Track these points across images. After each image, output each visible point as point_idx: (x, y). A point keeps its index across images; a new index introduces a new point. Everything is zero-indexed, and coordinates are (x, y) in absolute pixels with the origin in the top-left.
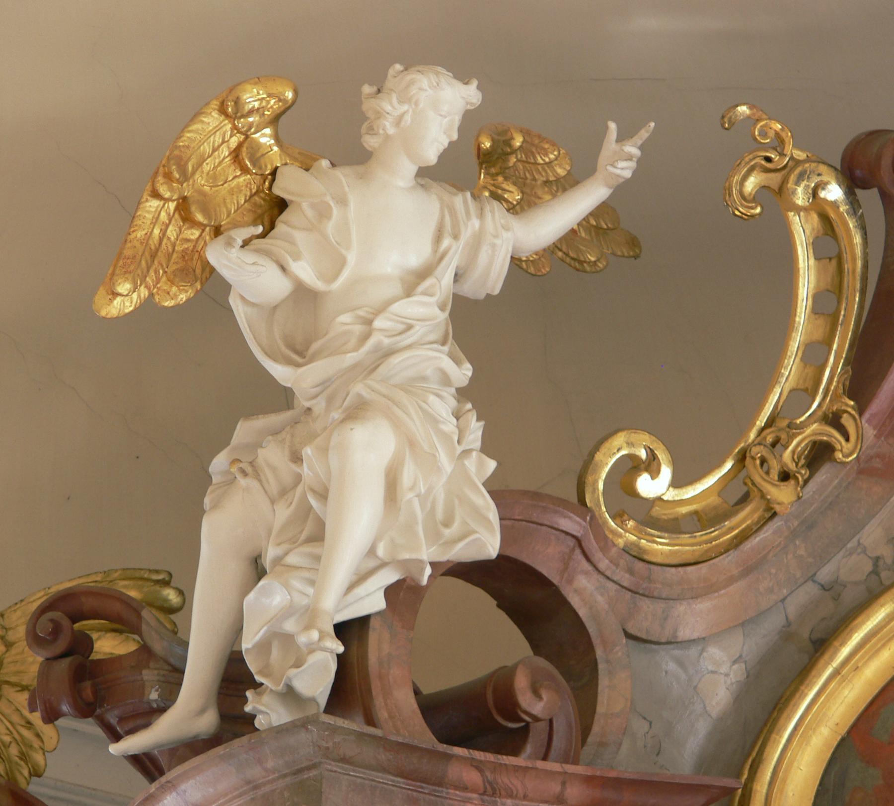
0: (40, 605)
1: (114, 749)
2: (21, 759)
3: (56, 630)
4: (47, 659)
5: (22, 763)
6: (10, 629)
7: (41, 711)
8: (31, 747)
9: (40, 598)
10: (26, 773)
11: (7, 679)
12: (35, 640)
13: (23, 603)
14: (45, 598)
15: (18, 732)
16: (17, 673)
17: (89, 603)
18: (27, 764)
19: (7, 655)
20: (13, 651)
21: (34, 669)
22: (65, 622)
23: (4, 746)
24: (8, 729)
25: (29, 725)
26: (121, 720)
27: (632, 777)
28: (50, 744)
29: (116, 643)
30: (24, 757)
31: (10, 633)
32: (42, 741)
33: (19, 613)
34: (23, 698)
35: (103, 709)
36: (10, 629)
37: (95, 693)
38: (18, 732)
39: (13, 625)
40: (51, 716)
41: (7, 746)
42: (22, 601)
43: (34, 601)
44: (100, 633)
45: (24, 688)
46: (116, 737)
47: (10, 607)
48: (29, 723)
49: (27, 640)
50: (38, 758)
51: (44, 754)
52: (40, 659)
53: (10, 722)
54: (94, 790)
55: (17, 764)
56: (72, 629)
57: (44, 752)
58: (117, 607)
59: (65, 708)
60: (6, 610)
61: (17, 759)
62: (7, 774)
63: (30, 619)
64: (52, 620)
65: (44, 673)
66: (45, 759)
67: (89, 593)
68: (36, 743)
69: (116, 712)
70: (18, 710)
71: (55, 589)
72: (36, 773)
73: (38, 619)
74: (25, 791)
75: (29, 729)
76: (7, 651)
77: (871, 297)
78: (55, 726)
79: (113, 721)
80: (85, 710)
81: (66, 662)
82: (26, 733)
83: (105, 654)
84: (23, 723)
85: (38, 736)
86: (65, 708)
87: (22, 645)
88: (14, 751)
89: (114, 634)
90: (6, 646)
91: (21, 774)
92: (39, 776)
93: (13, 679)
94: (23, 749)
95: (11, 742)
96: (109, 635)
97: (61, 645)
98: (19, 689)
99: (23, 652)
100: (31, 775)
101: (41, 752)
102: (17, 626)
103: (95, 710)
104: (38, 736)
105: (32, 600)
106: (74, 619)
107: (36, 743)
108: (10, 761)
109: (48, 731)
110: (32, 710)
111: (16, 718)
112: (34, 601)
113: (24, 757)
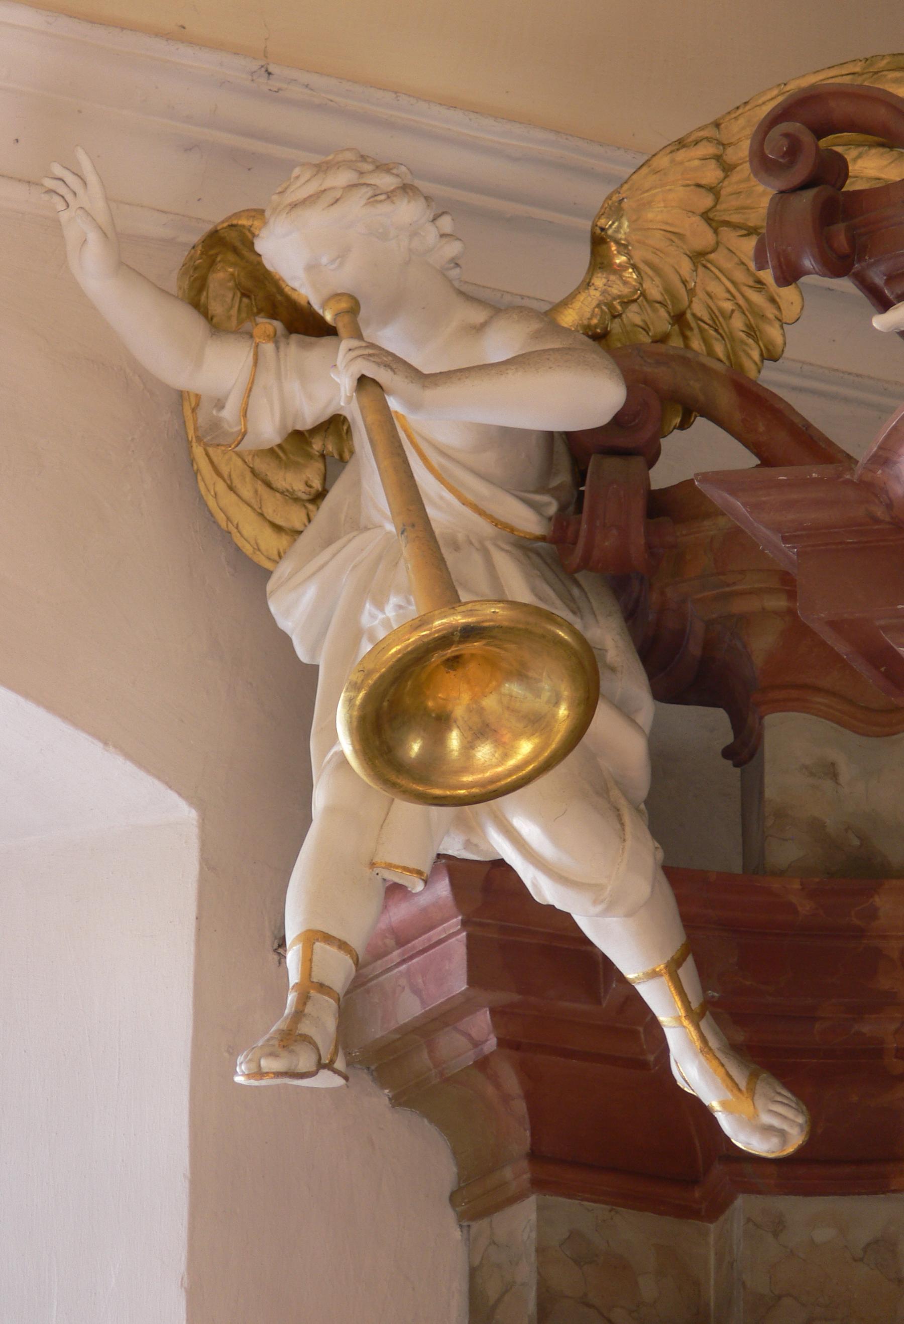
0: (773, 109)
1: (881, 322)
2: (748, 335)
3: (794, 150)
4: (782, 192)
5: (750, 341)
6: (730, 144)
7: (774, 268)
8: (763, 317)
9: (772, 99)
10: (756, 355)
11: (727, 219)
12: (764, 164)
13: (748, 107)
14: (780, 99)
15: (743, 296)
16: (741, 209)
17: (841, 109)
18: (757, 343)
19: (726, 183)
20: (735, 177)
21: (765, 202)
22: (807, 138)
23: (724, 317)
24: (729, 291)
25: (759, 284)
26: (891, 279)
27: (679, 1004)
28: (790, 313)
29: (885, 163)
30: (752, 332)
31: (730, 150)
32: (779, 308)
33: (742, 121)
34: (749, 245)
35: (864, 264)
36: (730, 144)
37: (852, 240)
38: (743, 296)
39: (733, 140)
40: (789, 275)
41: (728, 317)
42: (746, 103)
43: (764, 103)
44: (861, 149)
45: (751, 231)
46: (884, 305)
47: (729, 113)
48: (759, 282)
49: (751, 161)
50: (774, 333)
51: (782, 327)
52: (772, 192)
53: (733, 283)
54: (857, 376)
55: (743, 342)
56: (817, 147)
57: (782, 323)
58: (882, 114)
59: (808, 263)
60: (723, 117)
61: (743, 335)
62: (729, 358)
63: (756, 131)
64: (787, 135)
65: (777, 213)
66: (784, 335)
67: (841, 93)
68: (770, 311)
69: (883, 268)
70: (743, 263)
71: (793, 86)
72: (771, 355)
73: (766, 133)
74: (755, 383)
75: (759, 290)
76: (726, 177)
77: (307, 1085)
78: (797, 287)
79: (879, 280)
80: (838, 265)
81: (808, 196)
82: (756, 298)
83: (869, 179)
84: (751, 283)
85: (773, 300)
86: (808, 263)
87: (745, 169)
88: (738, 323)
89: (881, 150)
90: (724, 170)
91: (750, 357)
92: (776, 360)
93: (735, 218)
94: (752, 320)
95: (733, 311)
96: (874, 151)
97: (801, 171)
98: (745, 232)
99: (747, 180)
100: (763, 358)
101: (777, 324)
102: (740, 140)
103: (853, 265)
104: (773, 300)
105: (760, 102)
106: (820, 132)
107: (770, 311)
108: (732, 338)
109: (788, 294)
110: (761, 267)
111: (740, 276)
112: (764, 103)
113: (752, 332)
